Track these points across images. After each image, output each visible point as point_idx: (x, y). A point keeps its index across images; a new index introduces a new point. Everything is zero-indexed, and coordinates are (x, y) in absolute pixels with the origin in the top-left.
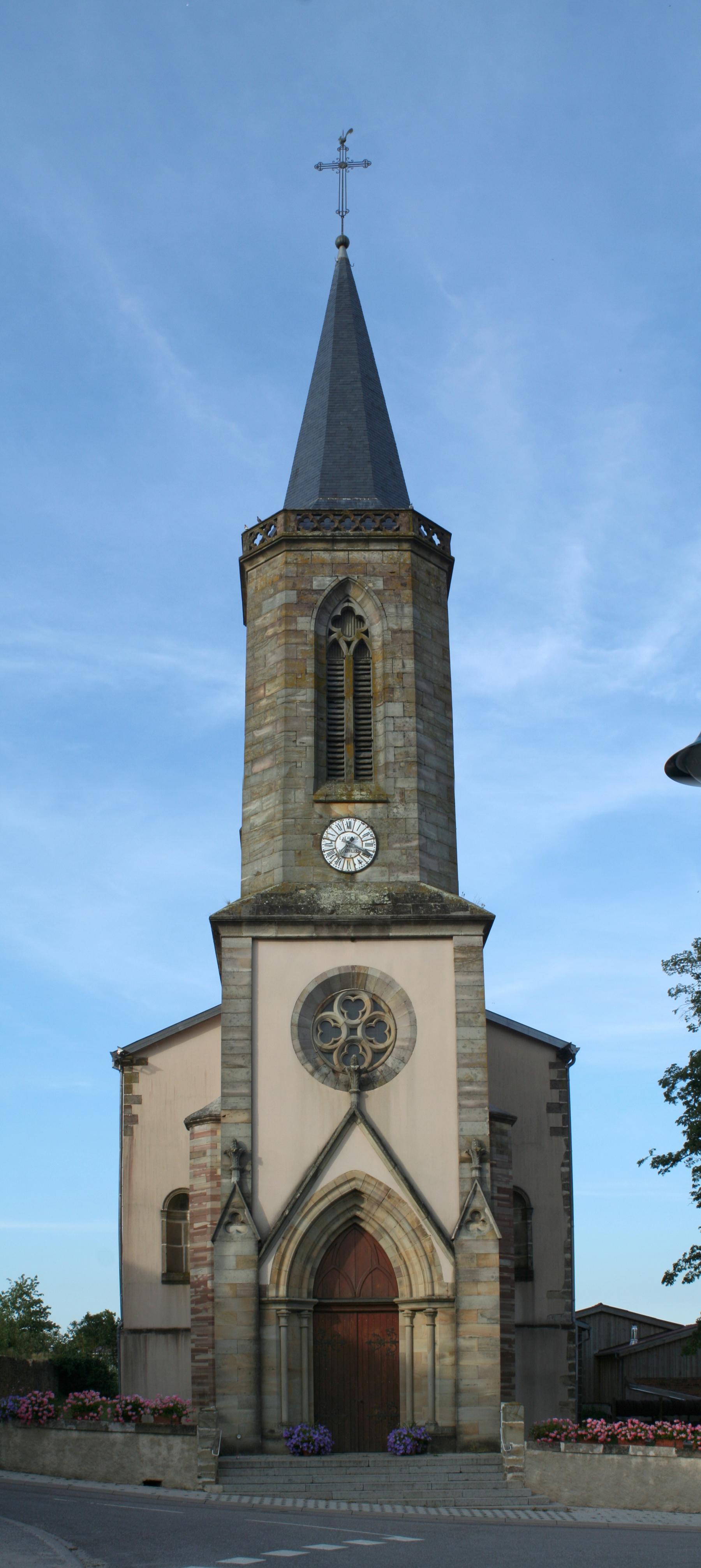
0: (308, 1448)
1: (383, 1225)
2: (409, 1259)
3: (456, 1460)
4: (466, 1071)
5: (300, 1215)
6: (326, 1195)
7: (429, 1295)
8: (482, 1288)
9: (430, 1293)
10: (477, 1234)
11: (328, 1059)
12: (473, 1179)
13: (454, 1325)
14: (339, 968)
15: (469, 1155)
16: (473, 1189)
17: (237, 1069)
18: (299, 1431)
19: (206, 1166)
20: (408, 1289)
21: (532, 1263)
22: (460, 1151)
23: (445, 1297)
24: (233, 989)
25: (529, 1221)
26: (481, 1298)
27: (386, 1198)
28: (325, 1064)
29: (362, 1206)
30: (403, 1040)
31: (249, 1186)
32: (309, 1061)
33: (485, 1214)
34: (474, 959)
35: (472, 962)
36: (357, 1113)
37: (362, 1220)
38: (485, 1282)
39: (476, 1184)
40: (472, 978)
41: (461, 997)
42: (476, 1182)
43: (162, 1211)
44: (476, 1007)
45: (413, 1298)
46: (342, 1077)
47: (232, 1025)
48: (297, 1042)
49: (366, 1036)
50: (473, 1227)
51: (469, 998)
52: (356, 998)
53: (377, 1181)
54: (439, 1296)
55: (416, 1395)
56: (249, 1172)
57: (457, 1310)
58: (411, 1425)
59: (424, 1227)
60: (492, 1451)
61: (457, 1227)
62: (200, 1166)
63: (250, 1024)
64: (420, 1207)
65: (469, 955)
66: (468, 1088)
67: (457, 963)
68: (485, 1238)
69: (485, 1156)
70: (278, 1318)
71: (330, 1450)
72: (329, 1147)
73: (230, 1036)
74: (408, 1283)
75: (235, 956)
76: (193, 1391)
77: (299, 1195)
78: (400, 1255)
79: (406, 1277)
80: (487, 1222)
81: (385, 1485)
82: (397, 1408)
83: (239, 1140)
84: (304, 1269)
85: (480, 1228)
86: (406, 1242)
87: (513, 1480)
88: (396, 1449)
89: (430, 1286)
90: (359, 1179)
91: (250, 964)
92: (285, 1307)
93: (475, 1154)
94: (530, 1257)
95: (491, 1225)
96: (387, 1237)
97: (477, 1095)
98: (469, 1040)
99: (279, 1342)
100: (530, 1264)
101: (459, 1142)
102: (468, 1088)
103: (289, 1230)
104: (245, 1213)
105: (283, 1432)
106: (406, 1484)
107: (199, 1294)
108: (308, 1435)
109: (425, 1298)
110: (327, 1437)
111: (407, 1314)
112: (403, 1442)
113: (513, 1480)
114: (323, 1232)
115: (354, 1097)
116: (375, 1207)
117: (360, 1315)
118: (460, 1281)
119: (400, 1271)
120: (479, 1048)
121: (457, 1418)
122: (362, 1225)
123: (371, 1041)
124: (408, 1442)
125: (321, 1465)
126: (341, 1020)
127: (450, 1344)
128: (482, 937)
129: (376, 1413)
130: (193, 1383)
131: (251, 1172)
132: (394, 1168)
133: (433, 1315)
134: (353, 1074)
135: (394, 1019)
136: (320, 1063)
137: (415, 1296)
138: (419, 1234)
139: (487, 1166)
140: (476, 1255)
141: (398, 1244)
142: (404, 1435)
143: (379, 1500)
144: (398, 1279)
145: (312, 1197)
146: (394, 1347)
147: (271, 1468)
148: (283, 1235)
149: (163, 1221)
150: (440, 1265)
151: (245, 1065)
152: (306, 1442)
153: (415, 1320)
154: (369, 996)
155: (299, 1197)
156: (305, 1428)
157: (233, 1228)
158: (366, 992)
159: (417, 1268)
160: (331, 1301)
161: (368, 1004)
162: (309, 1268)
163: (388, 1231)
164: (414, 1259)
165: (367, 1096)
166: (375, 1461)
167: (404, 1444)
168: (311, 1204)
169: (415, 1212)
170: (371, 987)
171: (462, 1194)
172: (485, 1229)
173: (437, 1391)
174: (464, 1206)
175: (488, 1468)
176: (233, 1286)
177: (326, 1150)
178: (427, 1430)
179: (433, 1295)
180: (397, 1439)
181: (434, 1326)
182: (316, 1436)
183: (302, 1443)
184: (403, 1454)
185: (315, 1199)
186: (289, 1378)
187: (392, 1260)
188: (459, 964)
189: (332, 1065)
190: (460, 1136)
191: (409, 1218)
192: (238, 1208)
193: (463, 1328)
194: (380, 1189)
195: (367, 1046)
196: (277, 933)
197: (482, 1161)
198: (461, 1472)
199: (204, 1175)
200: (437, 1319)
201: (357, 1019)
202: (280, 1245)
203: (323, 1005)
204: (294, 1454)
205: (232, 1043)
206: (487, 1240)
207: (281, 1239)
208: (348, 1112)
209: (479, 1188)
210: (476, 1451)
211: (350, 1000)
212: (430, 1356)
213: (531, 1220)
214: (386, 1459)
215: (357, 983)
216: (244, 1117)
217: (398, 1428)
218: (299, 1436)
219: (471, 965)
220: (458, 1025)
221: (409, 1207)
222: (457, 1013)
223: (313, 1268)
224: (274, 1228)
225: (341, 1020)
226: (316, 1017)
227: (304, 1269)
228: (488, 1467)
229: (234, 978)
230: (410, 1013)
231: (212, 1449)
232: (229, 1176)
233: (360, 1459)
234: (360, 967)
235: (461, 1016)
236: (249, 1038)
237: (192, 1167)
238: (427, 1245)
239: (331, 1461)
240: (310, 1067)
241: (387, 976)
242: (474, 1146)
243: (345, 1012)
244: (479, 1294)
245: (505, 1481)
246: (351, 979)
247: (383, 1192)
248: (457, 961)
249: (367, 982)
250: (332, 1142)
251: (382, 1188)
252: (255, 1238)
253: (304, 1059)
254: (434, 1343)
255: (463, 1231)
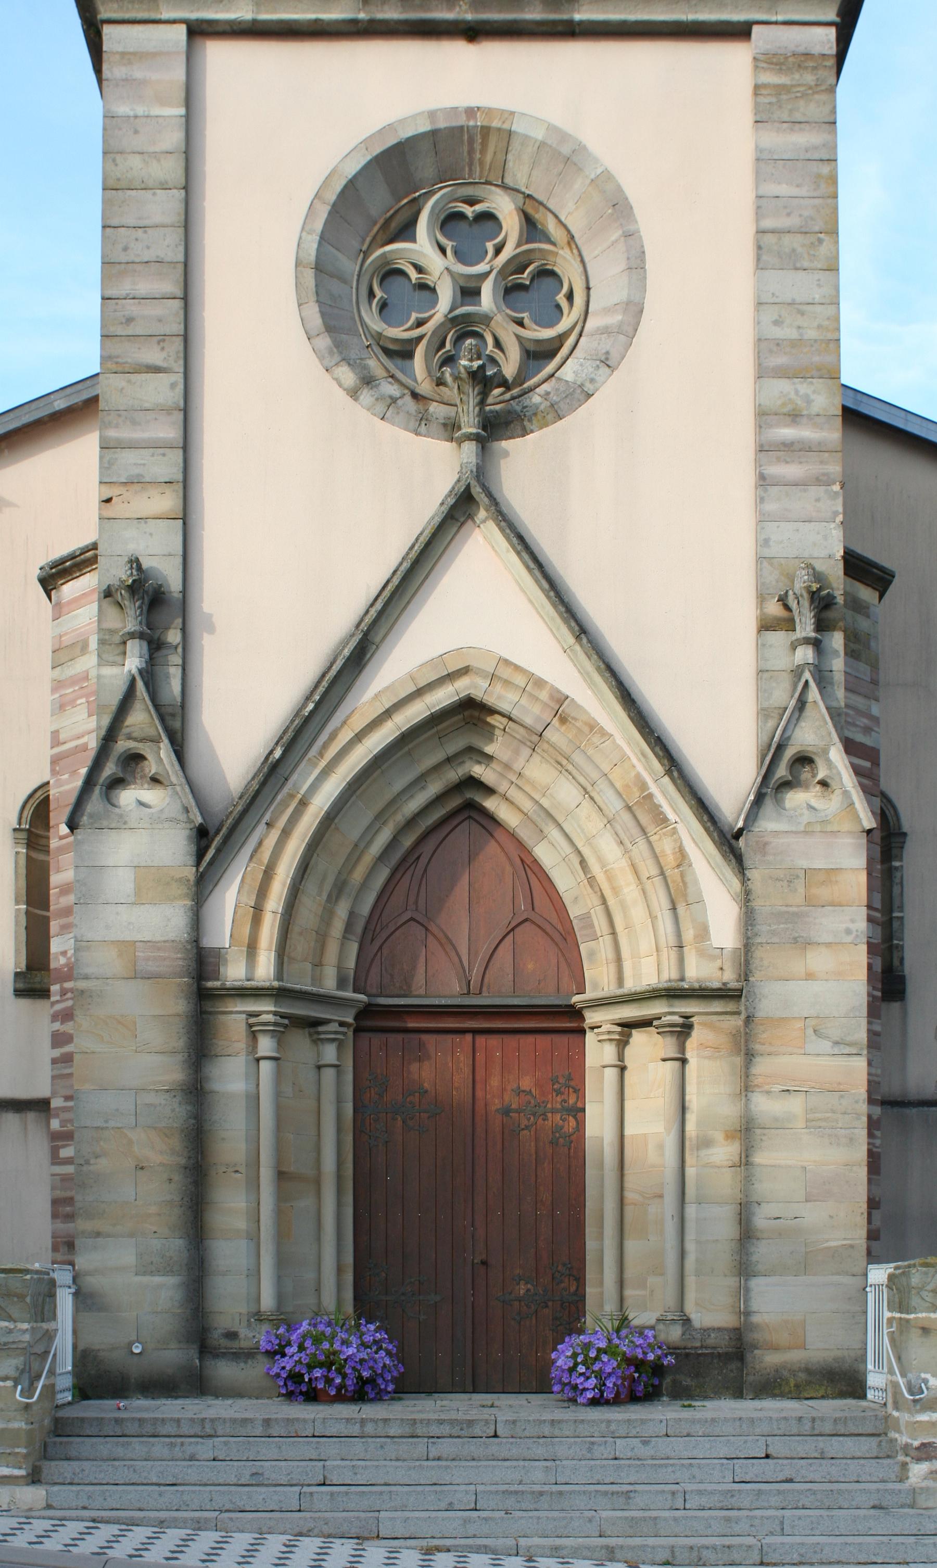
0: (329, 1381)
1: (545, 802)
2: (616, 890)
3: (752, 1421)
4: (780, 389)
5: (315, 765)
6: (388, 714)
7: (670, 981)
8: (818, 960)
9: (674, 975)
10: (807, 817)
11: (403, 371)
12: (797, 672)
13: (738, 1060)
14: (432, 114)
15: (787, 608)
16: (797, 695)
17: (144, 376)
18: (304, 1336)
19: (87, 678)
20: (612, 968)
21: (902, 960)
22: (761, 598)
23: (716, 985)
24: (135, 162)
25: (896, 864)
26: (816, 987)
27: (556, 722)
28: (392, 376)
29: (489, 749)
30: (607, 311)
31: (175, 686)
32: (346, 360)
33: (829, 762)
34: (810, 88)
35: (804, 95)
36: (476, 490)
37: (490, 791)
38: (828, 945)
39: (807, 682)
40: (803, 139)
41: (771, 189)
42: (807, 675)
43: (15, 830)
44: (812, 219)
45: (625, 990)
46: (435, 409)
47: (131, 258)
48: (313, 311)
49: (504, 308)
50: (795, 798)
51: (795, 191)
52: (478, 208)
53: (530, 676)
54: (698, 981)
55: (631, 1246)
56: (176, 647)
57: (749, 1020)
58: (616, 1323)
59: (660, 799)
60: (842, 1395)
61: (752, 797)
62: (73, 681)
63: (181, 257)
64: (649, 744)
65: (797, 76)
66: (787, 433)
67: (761, 100)
68: (829, 828)
69: (831, 614)
70: (253, 1036)
71: (391, 1388)
72: (396, 581)
73: (125, 287)
74: (611, 955)
75: (138, 73)
76: (54, 1236)
77: (311, 706)
78: (592, 881)
79: (608, 939)
80: (833, 784)
81: (541, 1494)
82: (580, 1280)
83: (146, 563)
84: (327, 916)
85: (813, 803)
86: (608, 847)
87: (930, 1483)
88: (575, 1387)
89: (673, 954)
90: (480, 672)
91: (183, 95)
92: (272, 1008)
93: (806, 603)
94: (897, 946)
95: (846, 794)
96: (555, 834)
97: (810, 450)
98: (792, 303)
99: (254, 1100)
100: (896, 962)
101: (759, 575)
102: (787, 433)
103: (285, 804)
104: (163, 754)
105: (262, 1336)
106: (606, 1493)
107: (69, 995)
108: (326, 1346)
109: (660, 986)
110: (383, 1353)
111: (609, 1032)
112: (597, 1367)
113: (930, 1483)
114: (380, 818)
115: (470, 448)
116: (526, 752)
117: (481, 1040)
118: (759, 940)
119: (592, 926)
120: (819, 327)
121: (746, 1306)
122: (490, 804)
123: (520, 323)
124: (608, 1369)
125: (356, 1429)
126: (436, 263)
127: (729, 1111)
128: (832, 32)
129: (522, 1292)
130: (55, 1216)
131: (180, 650)
132: (578, 638)
133: (684, 1030)
134: (468, 389)
135: (583, 261)
136: (379, 372)
137: (631, 985)
138: (645, 819)
139: (837, 640)
140: (802, 875)
141: (586, 851)
142: (599, 1350)
143: (523, 1542)
144: (583, 948)
145: (348, 717)
146: (572, 1123)
147: (210, 1436)
148: (267, 817)
149: (17, 853)
150: (700, 901)
151: (165, 365)
152: (321, 1365)
153: (628, 1051)
154: (514, 201)
155: (312, 713)
156: (321, 1328)
157: (127, 797)
158: (505, 187)
159: (638, 913)
160: (402, 1001)
161: (511, 224)
162: (342, 911)
163: (560, 819)
164: (630, 891)
165: (506, 454)
166: (514, 1422)
167: (599, 1375)
168: (345, 736)
169: (634, 761)
170: (518, 174)
171: (763, 713)
172: (830, 805)
173: (690, 1236)
174: (770, 745)
175: (849, 1446)
176: (127, 947)
177: (390, 587)
178: (662, 1337)
179: (682, 979)
180: (579, 1360)
181: (684, 1061)
182: (350, 1351)
183: (310, 1367)
184: (595, 1402)
185: (358, 723)
186: (282, 1197)
187: (567, 899)
188: (767, 100)
189: (413, 383)
190: (760, 559)
191: (615, 776)
192: (142, 740)
193: (761, 1067)
194: (537, 699)
195: (508, 334)
196: (258, 13)
197: (822, 626)
198: (767, 1457)
199: (83, 700)
200: (692, 1044)
201: (482, 264)
202: (260, 843)
203: (387, 222)
204: (290, 1396)
205: (131, 308)
206: (834, 833)
207: (262, 827)
208: (453, 488)
209: (814, 693)
210: (798, 1393)
211: (461, 216)
212: (671, 1142)
213: (901, 860)
214: (547, 1416)
215: (481, 163)
216: (167, 502)
217: (581, 1331)
218: (301, 1348)
219: (802, 103)
220: (760, 265)
221: (618, 747)
222: (760, 232)
223: (352, 914)
224: (240, 798)
225: (436, 263)
226: (366, 254)
227: (327, 916)
228: (849, 1442)
229: (136, 132)
230: (628, 235)
231: (16, 1382)
232: (119, 659)
233: (474, 1414)
234: (489, 112)
235: (770, 239)
236: (180, 293)
237: (58, 685)
238: (666, 847)
239: (386, 1421)
240: (348, 376)
241: (564, 136)
242: (801, 582)
243: (449, 245)
244: (810, 976)
245: (906, 1485)
246: (466, 148)
247: (546, 705)
248: (764, 92)
249: (510, 156)
250: (406, 565)
251: (544, 695)
252: (190, 821)
253: (331, 353)
254: (683, 1109)
255: (769, 805)
